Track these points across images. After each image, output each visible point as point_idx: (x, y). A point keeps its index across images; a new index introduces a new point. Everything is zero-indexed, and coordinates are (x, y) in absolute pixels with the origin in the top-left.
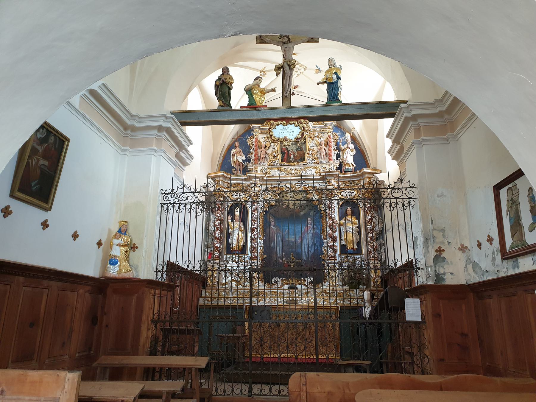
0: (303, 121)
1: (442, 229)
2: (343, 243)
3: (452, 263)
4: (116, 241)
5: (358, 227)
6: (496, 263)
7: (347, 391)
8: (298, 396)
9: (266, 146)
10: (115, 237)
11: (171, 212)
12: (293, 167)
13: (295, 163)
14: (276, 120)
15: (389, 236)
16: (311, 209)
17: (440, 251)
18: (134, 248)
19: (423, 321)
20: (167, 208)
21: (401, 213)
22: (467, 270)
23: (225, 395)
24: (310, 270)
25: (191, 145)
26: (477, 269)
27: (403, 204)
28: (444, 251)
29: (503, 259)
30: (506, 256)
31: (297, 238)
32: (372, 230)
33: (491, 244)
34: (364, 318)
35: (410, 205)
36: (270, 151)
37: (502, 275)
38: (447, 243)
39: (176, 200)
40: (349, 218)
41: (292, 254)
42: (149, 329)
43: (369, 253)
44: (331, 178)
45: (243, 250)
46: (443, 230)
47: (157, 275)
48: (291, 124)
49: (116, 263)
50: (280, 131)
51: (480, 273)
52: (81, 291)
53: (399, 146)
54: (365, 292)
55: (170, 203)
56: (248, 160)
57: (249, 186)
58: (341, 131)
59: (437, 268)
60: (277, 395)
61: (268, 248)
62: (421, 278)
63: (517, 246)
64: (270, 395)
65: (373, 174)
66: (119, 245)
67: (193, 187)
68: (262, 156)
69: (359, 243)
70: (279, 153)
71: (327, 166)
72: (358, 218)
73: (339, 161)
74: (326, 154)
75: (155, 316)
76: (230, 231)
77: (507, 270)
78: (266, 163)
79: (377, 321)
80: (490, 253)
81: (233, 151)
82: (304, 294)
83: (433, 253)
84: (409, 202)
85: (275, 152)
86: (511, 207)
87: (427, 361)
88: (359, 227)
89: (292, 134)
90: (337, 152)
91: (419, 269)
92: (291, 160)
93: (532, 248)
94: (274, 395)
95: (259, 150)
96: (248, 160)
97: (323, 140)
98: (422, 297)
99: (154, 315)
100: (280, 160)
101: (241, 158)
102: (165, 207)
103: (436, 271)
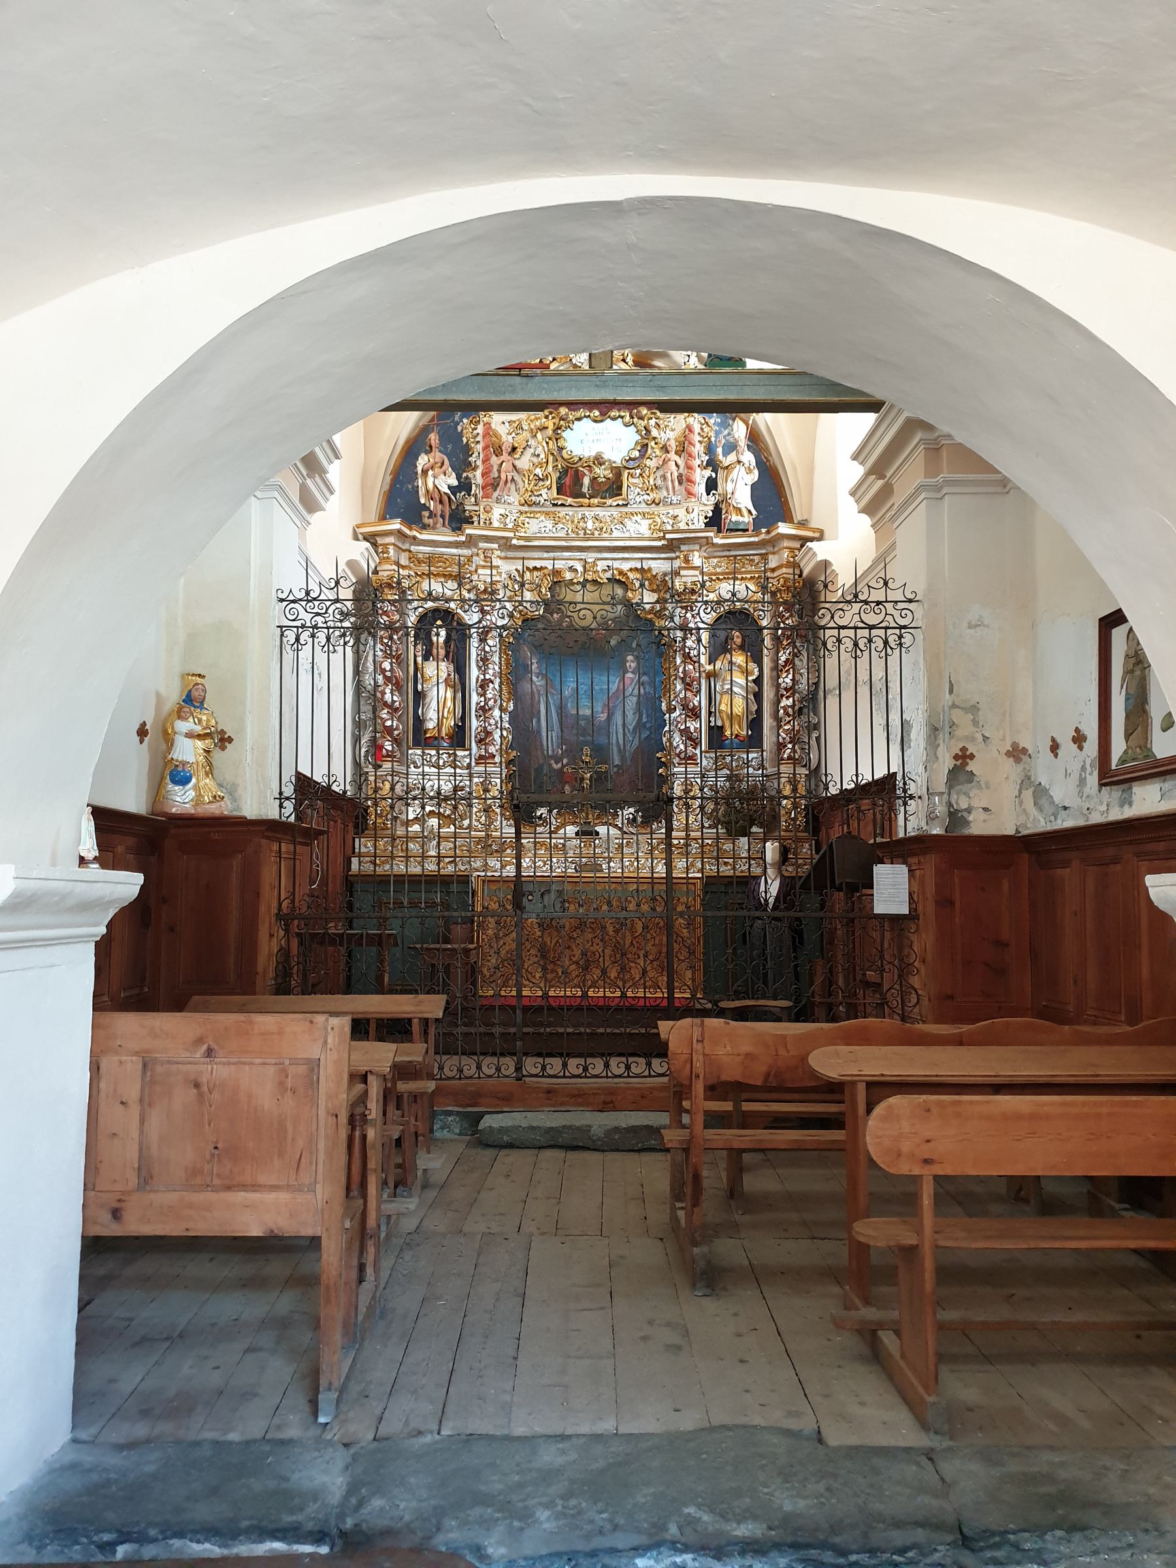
0: (644, 411)
3: (988, 787)
4: (183, 726)
5: (754, 681)
6: (1087, 791)
7: (782, 1052)
8: (686, 1062)
9: (514, 449)
10: (180, 715)
12: (590, 513)
13: (595, 501)
14: (572, 405)
15: (832, 702)
16: (635, 633)
17: (964, 757)
18: (224, 740)
19: (913, 916)
20: (297, 640)
21: (878, 665)
22: (1021, 803)
23: (460, 1078)
24: (658, 800)
25: (337, 462)
26: (1043, 801)
27: (886, 642)
28: (972, 757)
29: (1101, 785)
30: (1109, 777)
31: (598, 707)
32: (792, 690)
33: (1081, 748)
34: (762, 906)
35: (901, 645)
36: (524, 462)
37: (1096, 818)
38: (981, 738)
39: (319, 619)
40: (739, 659)
41: (587, 750)
42: (271, 936)
43: (781, 746)
44: (691, 547)
45: (458, 737)
46: (974, 709)
47: (281, 806)
48: (614, 419)
49: (188, 780)
51: (1049, 810)
52: (120, 849)
53: (880, 483)
54: (768, 844)
55: (303, 626)
56: (465, 486)
57: (470, 559)
59: (954, 797)
60: (579, 1076)
61: (522, 723)
62: (912, 821)
63: (1134, 760)
64: (564, 1077)
65: (804, 540)
66: (190, 735)
68: (503, 476)
69: (755, 723)
70: (550, 468)
71: (681, 512)
73: (712, 500)
74: (680, 476)
75: (285, 904)
77: (1107, 809)
78: (514, 498)
79: (792, 914)
80: (1075, 767)
81: (423, 461)
82: (625, 853)
83: (946, 763)
85: (540, 465)
86: (1132, 671)
87: (914, 1000)
88: (758, 681)
90: (708, 473)
91: (911, 797)
92: (585, 489)
93: (1163, 766)
94: (574, 1076)
95: (495, 460)
96: (465, 486)
98: (910, 860)
99: (280, 905)
101: (446, 481)
102: (291, 636)
103: (950, 805)
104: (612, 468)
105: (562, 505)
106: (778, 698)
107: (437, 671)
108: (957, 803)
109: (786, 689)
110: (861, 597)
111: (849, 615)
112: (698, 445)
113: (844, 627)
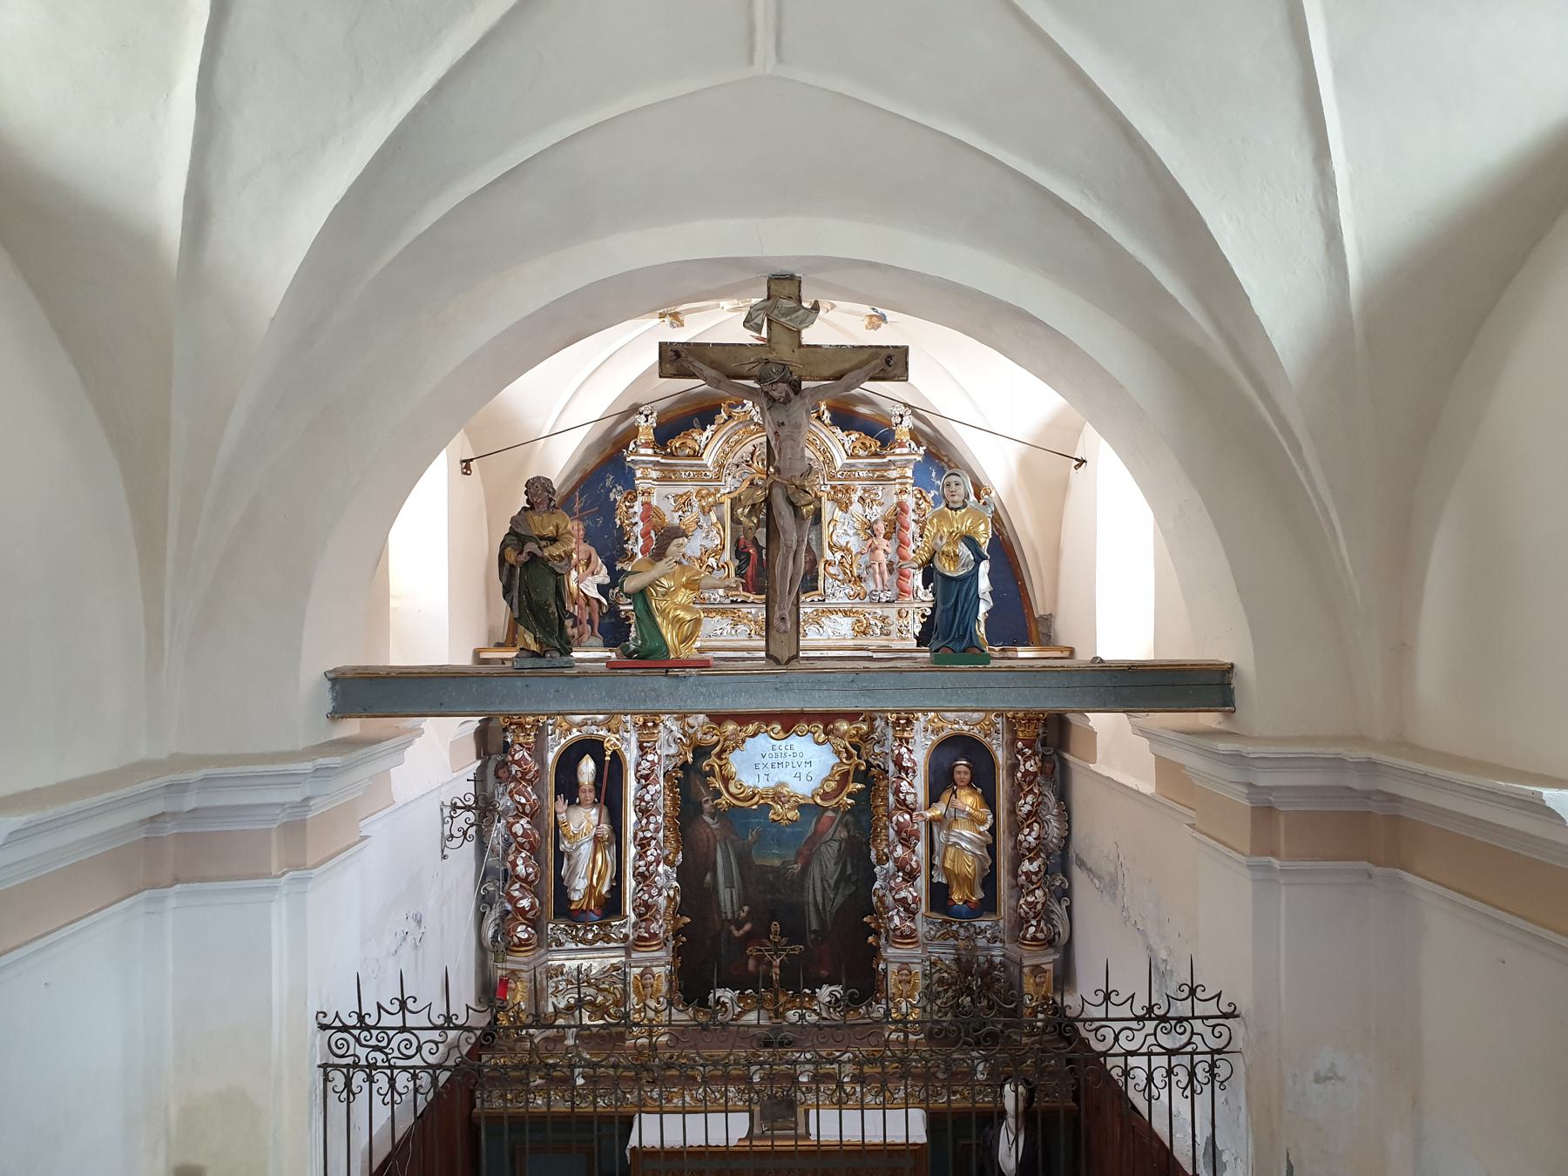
2: (940, 878)
11: (362, 1099)
14: (742, 719)
20: (348, 1084)
40: (968, 800)
45: (611, 905)
47: (326, 1080)
50: (758, 759)
55: (355, 1065)
61: (693, 876)
67: (439, 1008)
69: (989, 881)
72: (990, 801)
74: (890, 564)
76: (565, 845)
84: (1213, 1065)
89: (804, 770)
97: (876, 513)
102: (338, 1079)
104: (801, 807)
107: (584, 820)
109: (1029, 850)
110: (1157, 1012)
111: (1140, 1036)
113: (1133, 1053)
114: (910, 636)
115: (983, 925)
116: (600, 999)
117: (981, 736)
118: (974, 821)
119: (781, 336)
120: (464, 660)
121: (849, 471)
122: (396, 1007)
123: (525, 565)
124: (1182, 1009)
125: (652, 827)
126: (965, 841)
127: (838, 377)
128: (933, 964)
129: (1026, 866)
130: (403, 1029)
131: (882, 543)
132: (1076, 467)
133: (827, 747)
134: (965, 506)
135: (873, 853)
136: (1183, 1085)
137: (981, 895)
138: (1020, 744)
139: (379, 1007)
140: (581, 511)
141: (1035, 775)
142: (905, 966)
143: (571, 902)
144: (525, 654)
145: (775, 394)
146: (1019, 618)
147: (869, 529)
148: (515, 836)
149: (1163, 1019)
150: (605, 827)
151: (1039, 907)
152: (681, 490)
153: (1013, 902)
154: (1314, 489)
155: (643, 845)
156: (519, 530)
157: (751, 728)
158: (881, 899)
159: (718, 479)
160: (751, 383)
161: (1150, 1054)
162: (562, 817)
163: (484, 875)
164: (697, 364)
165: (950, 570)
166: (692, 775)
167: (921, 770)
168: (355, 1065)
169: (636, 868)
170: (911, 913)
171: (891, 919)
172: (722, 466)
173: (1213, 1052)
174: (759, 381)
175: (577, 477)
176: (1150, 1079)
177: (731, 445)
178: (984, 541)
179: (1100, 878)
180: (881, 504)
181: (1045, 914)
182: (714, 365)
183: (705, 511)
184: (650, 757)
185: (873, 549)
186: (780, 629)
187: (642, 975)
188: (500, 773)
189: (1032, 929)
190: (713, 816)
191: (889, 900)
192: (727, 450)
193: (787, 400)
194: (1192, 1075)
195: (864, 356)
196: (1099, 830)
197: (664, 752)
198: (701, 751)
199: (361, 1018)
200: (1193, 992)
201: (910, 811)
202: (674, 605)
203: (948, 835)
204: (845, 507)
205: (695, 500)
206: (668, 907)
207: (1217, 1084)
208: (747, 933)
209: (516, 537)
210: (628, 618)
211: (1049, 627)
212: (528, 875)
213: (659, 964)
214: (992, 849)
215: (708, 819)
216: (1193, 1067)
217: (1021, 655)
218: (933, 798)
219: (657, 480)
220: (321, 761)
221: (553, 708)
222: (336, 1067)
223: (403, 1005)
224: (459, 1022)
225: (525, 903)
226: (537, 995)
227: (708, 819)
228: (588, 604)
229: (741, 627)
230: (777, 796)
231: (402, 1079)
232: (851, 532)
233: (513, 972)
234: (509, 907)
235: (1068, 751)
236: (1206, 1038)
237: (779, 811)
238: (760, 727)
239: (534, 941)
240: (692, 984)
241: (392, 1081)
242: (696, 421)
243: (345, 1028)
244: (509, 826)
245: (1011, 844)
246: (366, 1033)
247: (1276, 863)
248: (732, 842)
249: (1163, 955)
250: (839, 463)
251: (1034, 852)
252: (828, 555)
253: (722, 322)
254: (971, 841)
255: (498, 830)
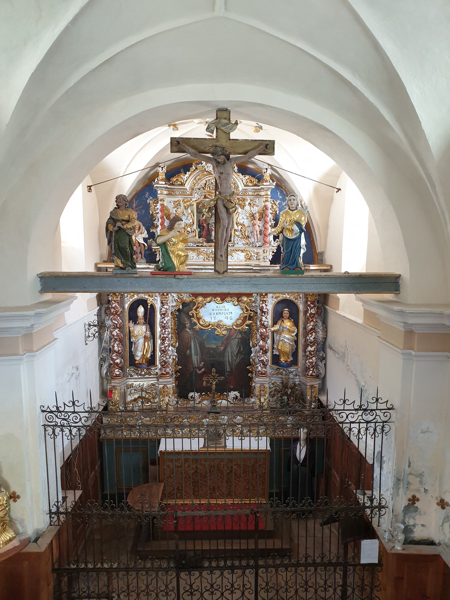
1: (421, 474)
3: (425, 513)
14: (205, 295)
17: (414, 500)
20: (54, 432)
22: (443, 530)
28: (418, 500)
38: (423, 490)
40: (288, 324)
45: (151, 362)
46: (421, 475)
47: (45, 430)
55: (56, 425)
58: (282, 193)
69: (295, 354)
72: (296, 324)
74: (260, 231)
76: (133, 339)
84: (383, 427)
89: (229, 316)
97: (255, 210)
99: (53, 565)
100: (197, 236)
102: (50, 430)
104: (227, 329)
105: (201, 246)
106: (306, 346)
107: (140, 330)
108: (408, 522)
109: (311, 343)
111: (356, 416)
112: (270, 215)
114: (268, 260)
115: (292, 370)
116: (147, 396)
117: (294, 300)
118: (290, 331)
119: (222, 135)
120: (91, 269)
121: (245, 191)
122: (71, 404)
123: (117, 231)
124: (374, 407)
125: (167, 333)
126: (286, 339)
127: (245, 153)
128: (273, 384)
129: (309, 348)
130: (74, 412)
131: (258, 222)
132: (337, 192)
133: (238, 307)
134: (296, 209)
135: (251, 343)
136: (371, 434)
137: (291, 359)
138: (309, 303)
139: (65, 404)
140: (136, 207)
141: (314, 314)
142: (262, 385)
143: (136, 360)
144: (117, 268)
145: (219, 160)
146: (313, 256)
147: (253, 216)
148: (114, 336)
149: (365, 410)
150: (148, 333)
151: (314, 363)
152: (176, 199)
153: (304, 362)
154: (439, 204)
155: (163, 340)
156: (113, 217)
157: (208, 299)
158: (253, 360)
159: (191, 195)
160: (209, 155)
161: (359, 423)
162: (132, 329)
163: (102, 349)
164: (187, 147)
165: (290, 236)
166: (182, 313)
167: (270, 313)
168: (56, 425)
169: (160, 348)
170: (265, 365)
171: (257, 367)
172: (193, 189)
173: (383, 422)
174: (213, 154)
175: (134, 193)
176: (359, 432)
177: (197, 180)
178: (304, 224)
179: (338, 354)
180: (257, 206)
181: (315, 366)
182: (193, 147)
183: (186, 208)
184: (166, 307)
185: (254, 225)
186: (220, 257)
187: (163, 388)
188: (107, 312)
189: (311, 372)
190: (190, 329)
191: (257, 360)
192: (197, 182)
193: (224, 163)
194: (375, 430)
195: (256, 144)
196: (337, 335)
197: (171, 304)
198: (184, 304)
199: (57, 408)
200: (377, 400)
201: (266, 328)
202: (177, 249)
203: (280, 337)
204: (243, 207)
205: (181, 203)
206: (173, 363)
207: (384, 434)
208: (203, 372)
209: (112, 220)
210: (155, 252)
211: (322, 257)
212: (119, 350)
213: (170, 383)
214: (296, 342)
215: (188, 330)
216: (376, 427)
217: (311, 268)
218: (275, 323)
219: (167, 195)
220: (38, 311)
221: (130, 290)
222: (49, 426)
223: (74, 403)
224: (96, 410)
225: (118, 361)
226: (124, 395)
227: (188, 330)
228: (139, 246)
229: (201, 256)
230: (219, 326)
231: (74, 431)
232: (245, 218)
233: (114, 386)
234: (112, 362)
235: (327, 305)
236: (381, 417)
237: (219, 332)
238: (212, 299)
239: (122, 375)
240: (182, 392)
241: (70, 431)
242: (182, 170)
243: (51, 412)
244: (111, 332)
245: (304, 340)
246: (60, 414)
247: (413, 353)
248: (197, 339)
249: (363, 384)
250: (240, 189)
251: (312, 343)
252: (236, 227)
253: (196, 129)
254: (288, 339)
255: (106, 335)
